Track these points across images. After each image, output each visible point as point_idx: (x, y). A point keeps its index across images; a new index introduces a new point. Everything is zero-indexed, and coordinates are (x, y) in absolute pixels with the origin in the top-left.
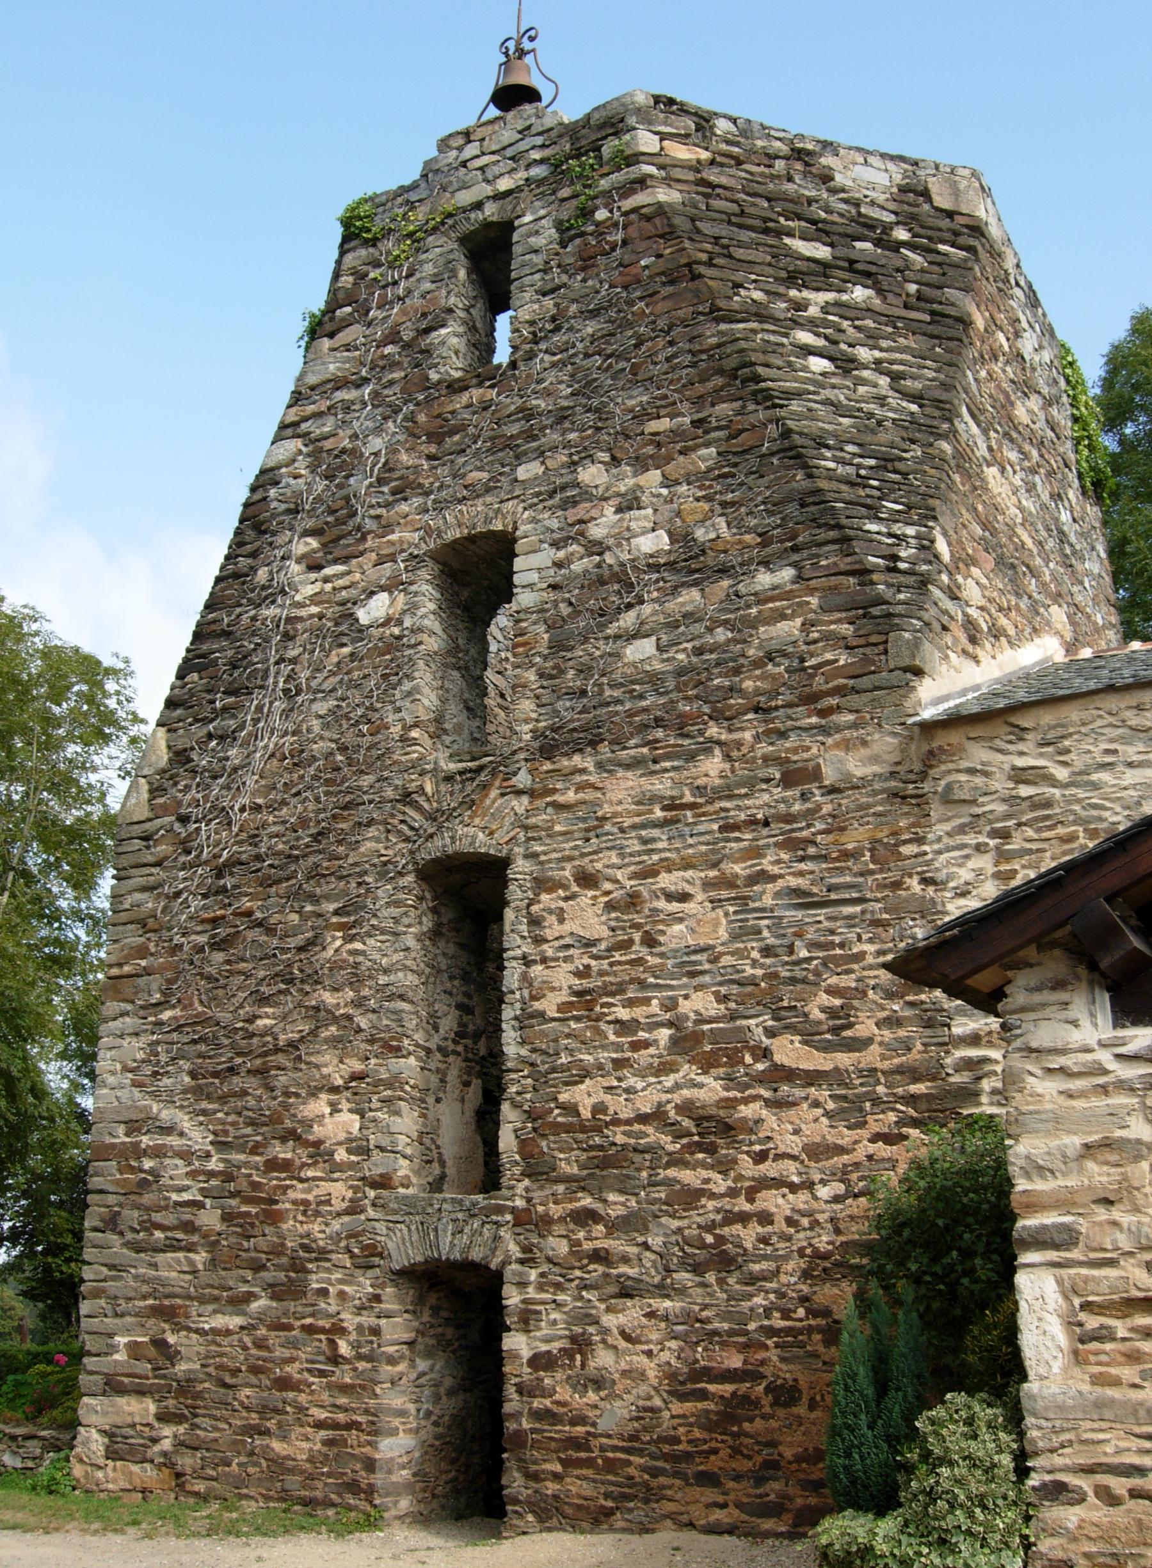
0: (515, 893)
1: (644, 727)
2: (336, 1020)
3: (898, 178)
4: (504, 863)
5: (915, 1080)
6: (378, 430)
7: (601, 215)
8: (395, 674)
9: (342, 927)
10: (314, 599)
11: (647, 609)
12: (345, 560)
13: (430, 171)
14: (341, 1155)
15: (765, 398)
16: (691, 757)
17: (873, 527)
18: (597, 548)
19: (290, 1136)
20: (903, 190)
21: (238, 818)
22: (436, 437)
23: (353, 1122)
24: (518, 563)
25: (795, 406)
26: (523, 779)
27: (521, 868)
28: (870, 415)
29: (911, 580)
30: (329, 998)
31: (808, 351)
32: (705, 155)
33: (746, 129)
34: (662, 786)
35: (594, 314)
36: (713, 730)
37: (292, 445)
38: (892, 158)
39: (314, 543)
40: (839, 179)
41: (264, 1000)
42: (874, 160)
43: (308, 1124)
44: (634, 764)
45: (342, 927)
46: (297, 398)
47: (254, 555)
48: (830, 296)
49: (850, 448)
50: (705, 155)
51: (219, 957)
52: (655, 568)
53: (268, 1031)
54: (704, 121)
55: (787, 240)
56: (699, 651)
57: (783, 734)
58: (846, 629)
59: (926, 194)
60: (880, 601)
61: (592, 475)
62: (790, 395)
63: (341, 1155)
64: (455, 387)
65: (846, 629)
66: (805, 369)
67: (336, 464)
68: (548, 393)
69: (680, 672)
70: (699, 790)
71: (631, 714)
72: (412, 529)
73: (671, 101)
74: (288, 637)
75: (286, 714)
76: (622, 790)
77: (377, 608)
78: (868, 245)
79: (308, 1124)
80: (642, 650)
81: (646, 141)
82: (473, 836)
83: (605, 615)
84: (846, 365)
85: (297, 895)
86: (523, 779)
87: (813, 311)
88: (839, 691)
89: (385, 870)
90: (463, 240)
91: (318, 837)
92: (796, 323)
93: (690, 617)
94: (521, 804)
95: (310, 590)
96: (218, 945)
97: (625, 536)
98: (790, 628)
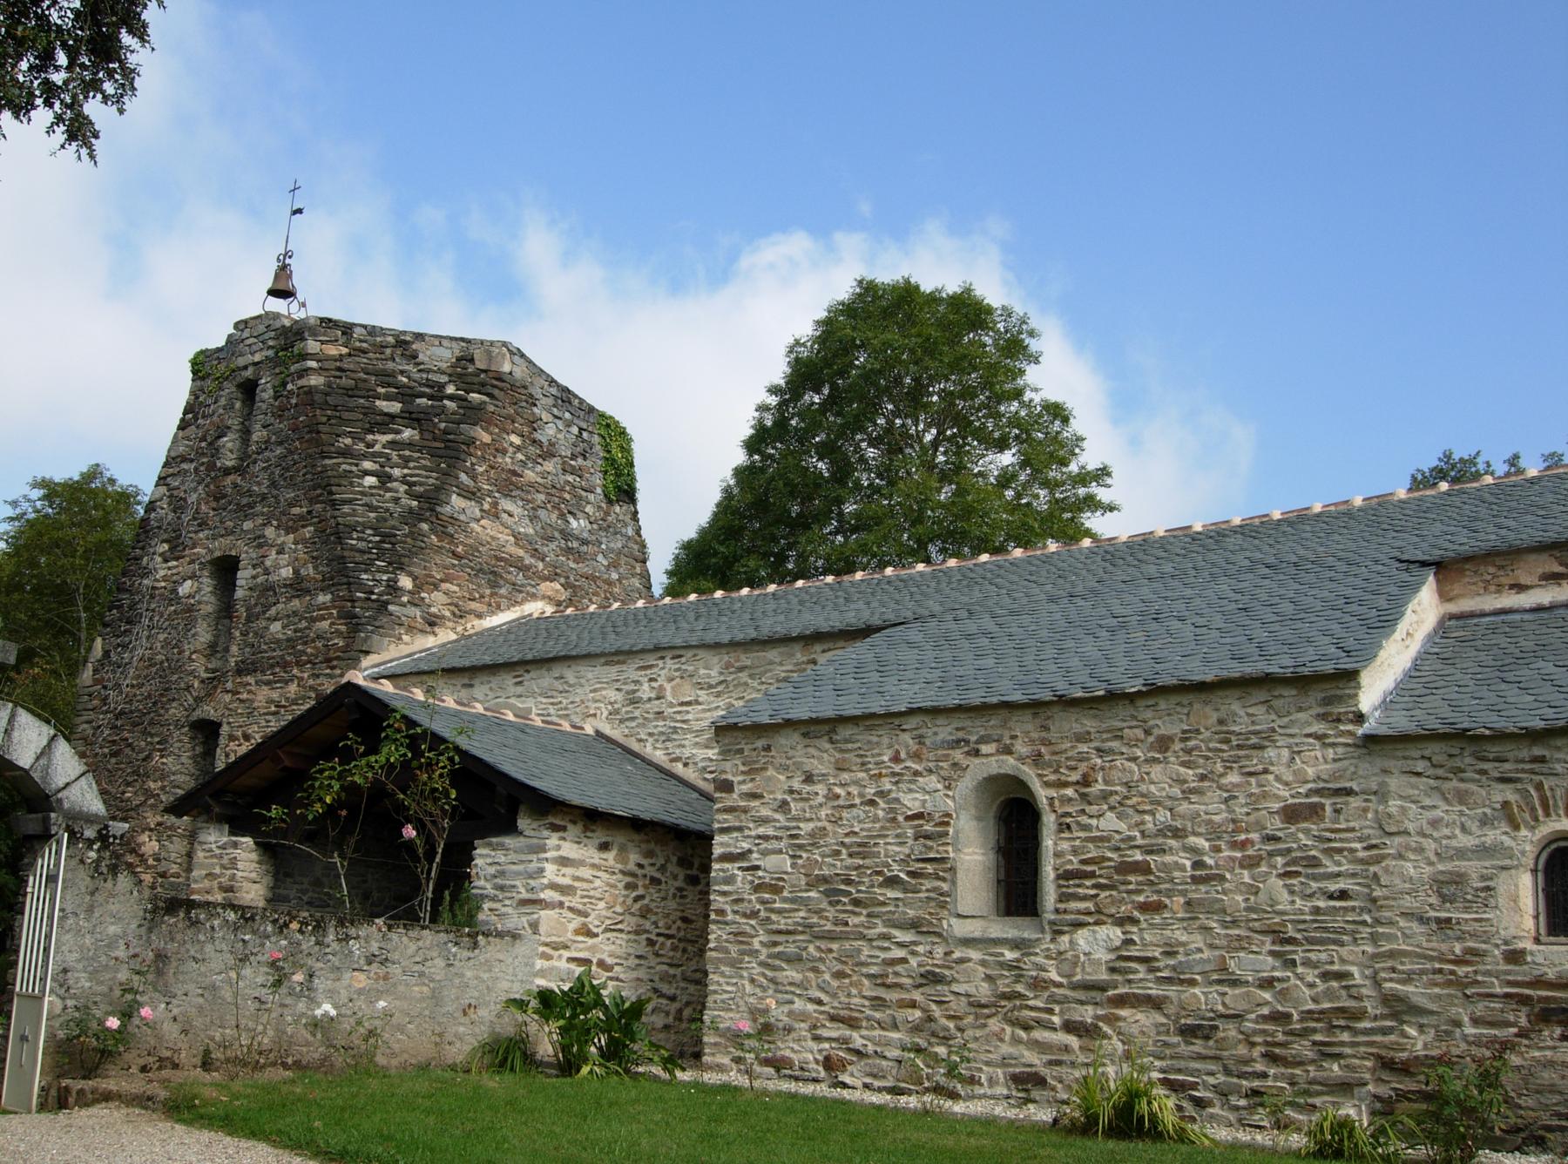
0: (222, 741)
1: (272, 666)
2: (153, 796)
3: (457, 353)
4: (219, 725)
5: (442, 898)
6: (195, 490)
7: (290, 387)
8: (190, 624)
9: (160, 750)
10: (165, 578)
11: (280, 606)
12: (177, 559)
13: (230, 340)
14: (150, 862)
15: (334, 504)
16: (286, 682)
17: (365, 576)
18: (267, 572)
19: (133, 851)
20: (459, 359)
21: (126, 690)
22: (217, 499)
23: (155, 845)
24: (239, 574)
25: (346, 509)
26: (229, 685)
27: (225, 729)
28: (387, 510)
29: (375, 605)
30: (152, 785)
31: (367, 473)
32: (345, 351)
33: (372, 331)
34: (275, 695)
35: (281, 443)
36: (295, 671)
37: (163, 489)
38: (456, 339)
39: (166, 546)
40: (421, 357)
41: (128, 784)
42: (445, 343)
43: (139, 845)
44: (268, 683)
45: (160, 750)
46: (166, 465)
47: (143, 548)
48: (389, 437)
49: (369, 532)
50: (345, 351)
51: (113, 760)
52: (285, 586)
53: (128, 800)
54: (347, 329)
55: (378, 403)
56: (295, 631)
57: (318, 676)
58: (343, 628)
59: (472, 360)
60: (355, 616)
61: (270, 532)
62: (345, 502)
63: (150, 862)
64: (227, 472)
65: (343, 628)
66: (360, 485)
67: (178, 504)
68: (259, 484)
69: (288, 640)
70: (287, 699)
71: (269, 658)
72: (207, 546)
73: (330, 320)
74: (152, 597)
75: (148, 638)
76: (263, 694)
77: (186, 588)
78: (424, 400)
79: (139, 845)
80: (276, 627)
81: (312, 346)
82: (209, 711)
83: (267, 607)
84: (385, 478)
85: (145, 733)
86: (229, 685)
87: (377, 448)
88: (338, 658)
89: (178, 726)
90: (239, 386)
91: (155, 704)
92: (365, 456)
93: (295, 613)
94: (228, 697)
95: (162, 573)
96: (114, 754)
97: (277, 567)
98: (325, 624)
